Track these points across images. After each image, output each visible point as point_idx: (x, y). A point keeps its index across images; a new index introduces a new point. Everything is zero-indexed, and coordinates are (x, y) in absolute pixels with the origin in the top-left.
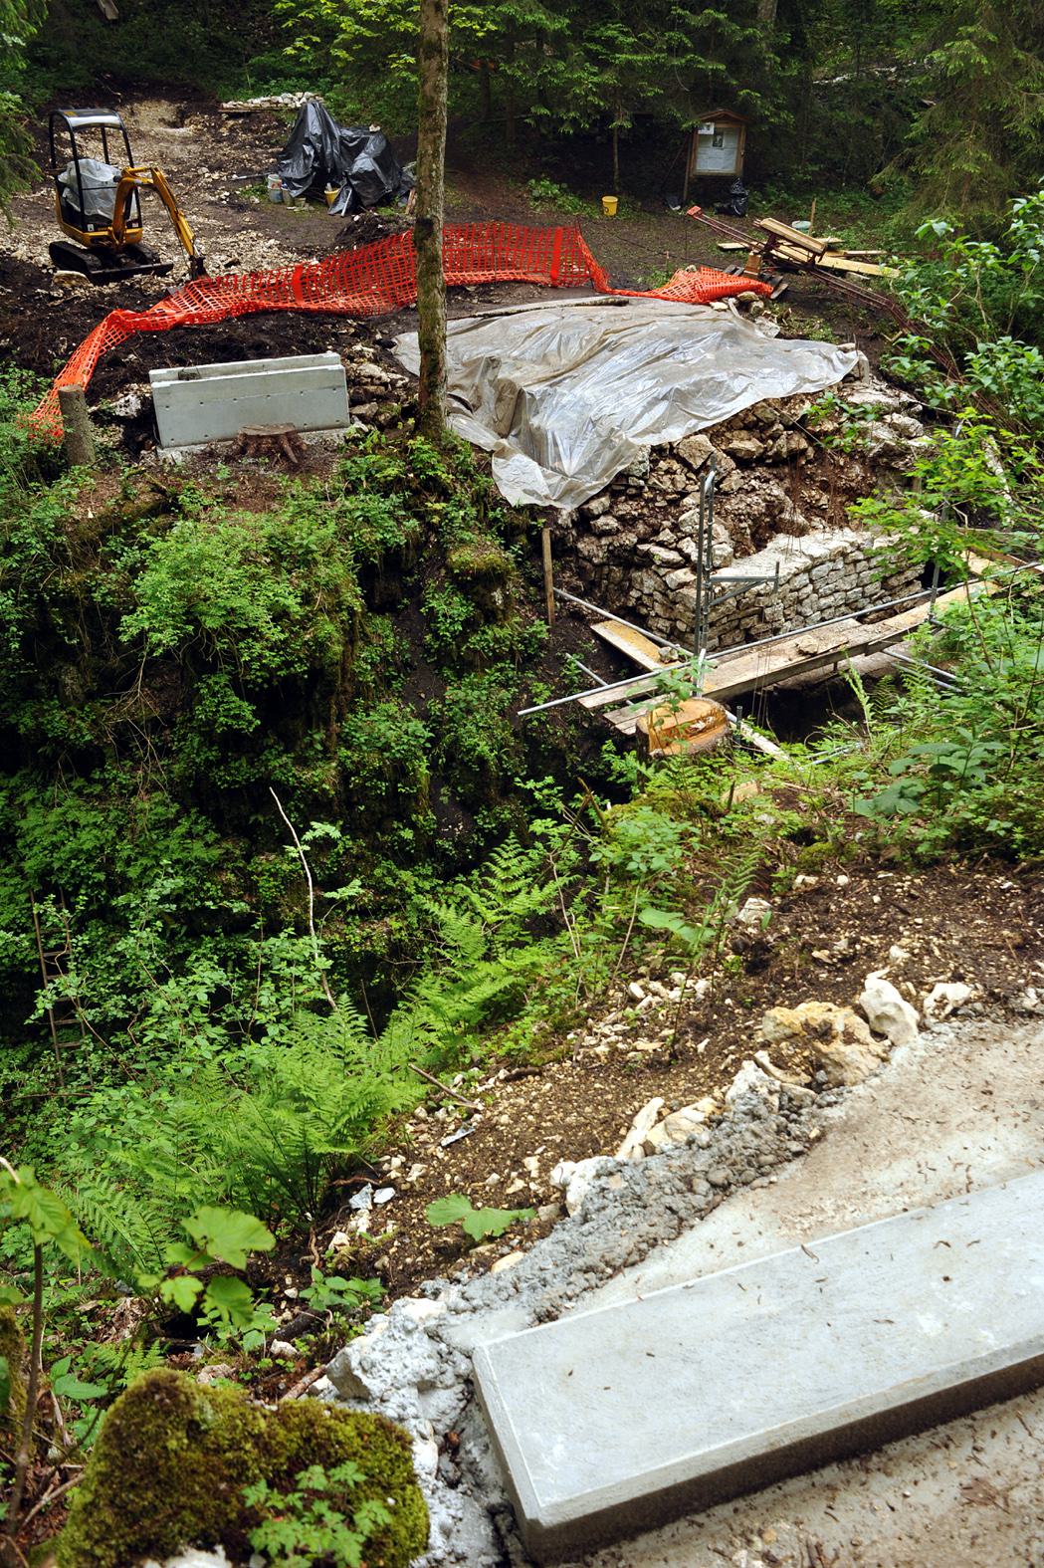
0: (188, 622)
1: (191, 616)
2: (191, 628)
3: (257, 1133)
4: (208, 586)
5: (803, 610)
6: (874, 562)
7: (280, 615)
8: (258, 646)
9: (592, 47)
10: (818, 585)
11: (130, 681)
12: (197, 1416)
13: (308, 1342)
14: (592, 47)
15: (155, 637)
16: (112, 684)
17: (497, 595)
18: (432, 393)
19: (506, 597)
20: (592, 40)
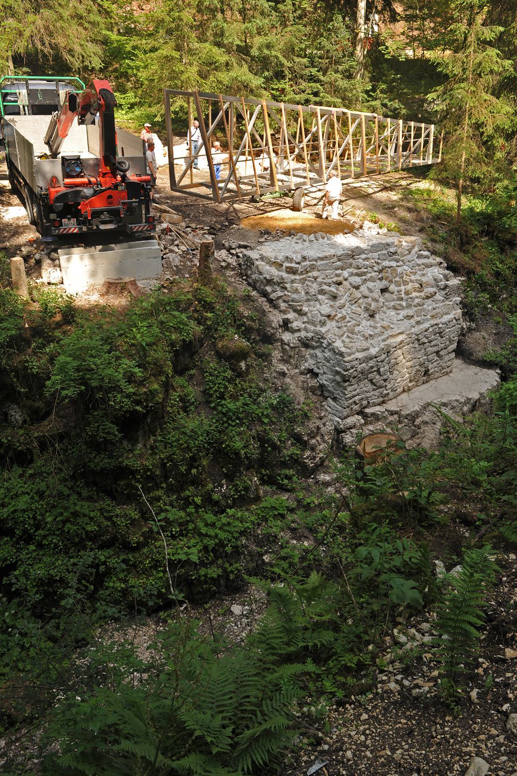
0: (81, 384)
2: (83, 388)
3: (259, 720)
4: (91, 362)
6: (433, 343)
7: (130, 378)
8: (119, 396)
11: (48, 414)
16: (36, 416)
17: (243, 365)
18: (206, 260)
19: (247, 365)
20: (273, 89)
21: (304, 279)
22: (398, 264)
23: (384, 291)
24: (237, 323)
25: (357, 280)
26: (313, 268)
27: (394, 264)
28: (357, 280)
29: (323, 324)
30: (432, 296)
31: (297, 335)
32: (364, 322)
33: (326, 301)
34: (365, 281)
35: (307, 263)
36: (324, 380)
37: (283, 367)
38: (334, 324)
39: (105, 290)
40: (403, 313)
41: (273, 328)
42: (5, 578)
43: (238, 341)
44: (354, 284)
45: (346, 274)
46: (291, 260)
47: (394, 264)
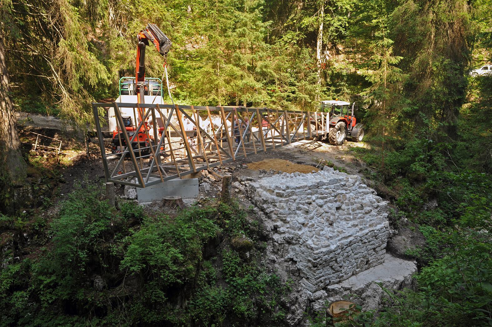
0: (144, 263)
1: (145, 261)
2: (144, 266)
4: (151, 249)
5: (349, 259)
6: (371, 243)
7: (175, 261)
9: (269, 91)
10: (354, 251)
12: (79, 292)
13: (92, 234)
14: (269, 91)
15: (132, 268)
16: (112, 284)
17: (248, 254)
18: (226, 187)
19: (250, 255)
20: (268, 90)
21: (288, 201)
22: (347, 192)
23: (338, 208)
24: (244, 226)
25: (321, 202)
26: (293, 193)
27: (344, 192)
28: (321, 202)
29: (300, 229)
31: (283, 236)
37: (273, 257)
38: (307, 229)
41: (268, 231)
44: (319, 204)
45: (314, 197)
46: (279, 188)
47: (344, 192)
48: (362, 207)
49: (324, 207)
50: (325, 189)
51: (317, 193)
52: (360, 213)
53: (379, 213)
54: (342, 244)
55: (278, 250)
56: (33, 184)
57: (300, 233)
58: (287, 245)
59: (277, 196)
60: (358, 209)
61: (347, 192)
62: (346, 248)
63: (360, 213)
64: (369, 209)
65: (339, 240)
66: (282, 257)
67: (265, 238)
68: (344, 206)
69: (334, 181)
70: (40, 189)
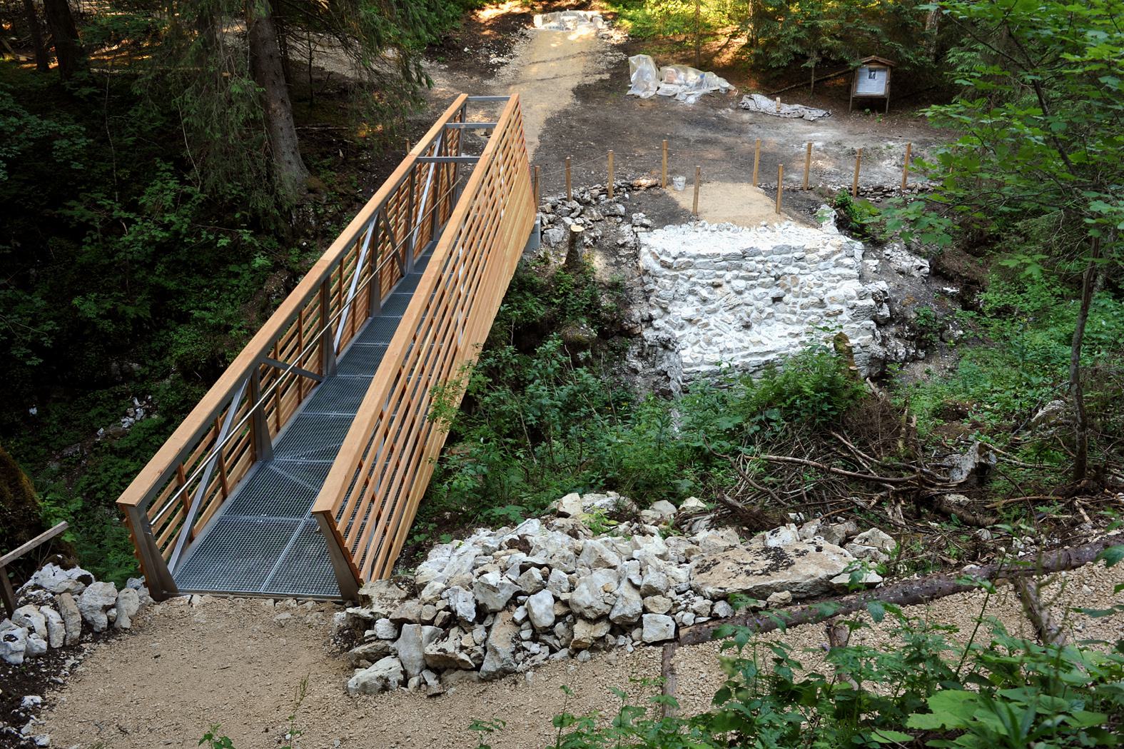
21: (676, 277)
22: (802, 272)
23: (777, 300)
24: (592, 311)
25: (741, 284)
26: (690, 265)
27: (796, 271)
28: (741, 284)
29: (682, 327)
30: (837, 315)
31: (657, 333)
32: (734, 333)
33: (696, 303)
34: (753, 287)
35: (686, 259)
36: (673, 385)
37: (638, 364)
38: (694, 329)
39: (859, 70)
40: (791, 329)
41: (632, 322)
42: (46, 345)
43: (584, 331)
44: (736, 288)
45: (729, 275)
46: (668, 255)
47: (796, 271)
48: (821, 304)
49: (746, 294)
50: (758, 262)
51: (739, 267)
52: (813, 313)
53: (855, 318)
54: (747, 364)
55: (648, 354)
56: (316, 205)
57: (678, 333)
58: (661, 349)
59: (662, 266)
60: (813, 305)
61: (802, 272)
62: (755, 371)
63: (813, 313)
64: (836, 307)
65: (744, 357)
66: (653, 365)
67: (629, 334)
68: (788, 298)
69: (782, 249)
70: (326, 212)
